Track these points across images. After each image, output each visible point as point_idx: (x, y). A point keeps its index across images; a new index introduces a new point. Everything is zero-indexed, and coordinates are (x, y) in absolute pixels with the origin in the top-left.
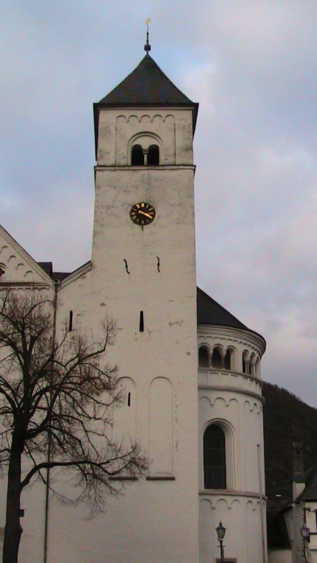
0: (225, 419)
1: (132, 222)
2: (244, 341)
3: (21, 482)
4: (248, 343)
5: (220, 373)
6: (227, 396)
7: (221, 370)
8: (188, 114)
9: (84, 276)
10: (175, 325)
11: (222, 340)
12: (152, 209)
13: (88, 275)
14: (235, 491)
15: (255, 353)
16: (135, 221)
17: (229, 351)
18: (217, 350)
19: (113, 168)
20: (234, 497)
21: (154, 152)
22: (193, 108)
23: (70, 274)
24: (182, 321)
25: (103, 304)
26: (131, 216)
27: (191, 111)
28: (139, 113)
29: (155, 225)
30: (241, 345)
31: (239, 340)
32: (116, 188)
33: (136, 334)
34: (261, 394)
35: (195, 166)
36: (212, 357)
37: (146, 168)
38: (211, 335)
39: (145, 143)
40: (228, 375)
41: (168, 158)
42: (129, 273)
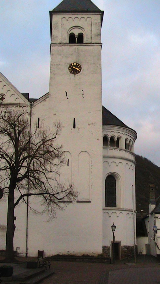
2: (126, 134)
3: (15, 203)
4: (128, 134)
6: (117, 161)
16: (71, 72)
17: (118, 139)
18: (112, 138)
19: (60, 45)
20: (119, 211)
21: (81, 36)
22: (101, 14)
24: (95, 123)
25: (55, 115)
26: (69, 69)
27: (100, 15)
28: (73, 16)
29: (81, 74)
32: (61, 55)
33: (71, 130)
35: (102, 44)
36: (110, 141)
39: (76, 32)
40: (118, 150)
42: (68, 99)
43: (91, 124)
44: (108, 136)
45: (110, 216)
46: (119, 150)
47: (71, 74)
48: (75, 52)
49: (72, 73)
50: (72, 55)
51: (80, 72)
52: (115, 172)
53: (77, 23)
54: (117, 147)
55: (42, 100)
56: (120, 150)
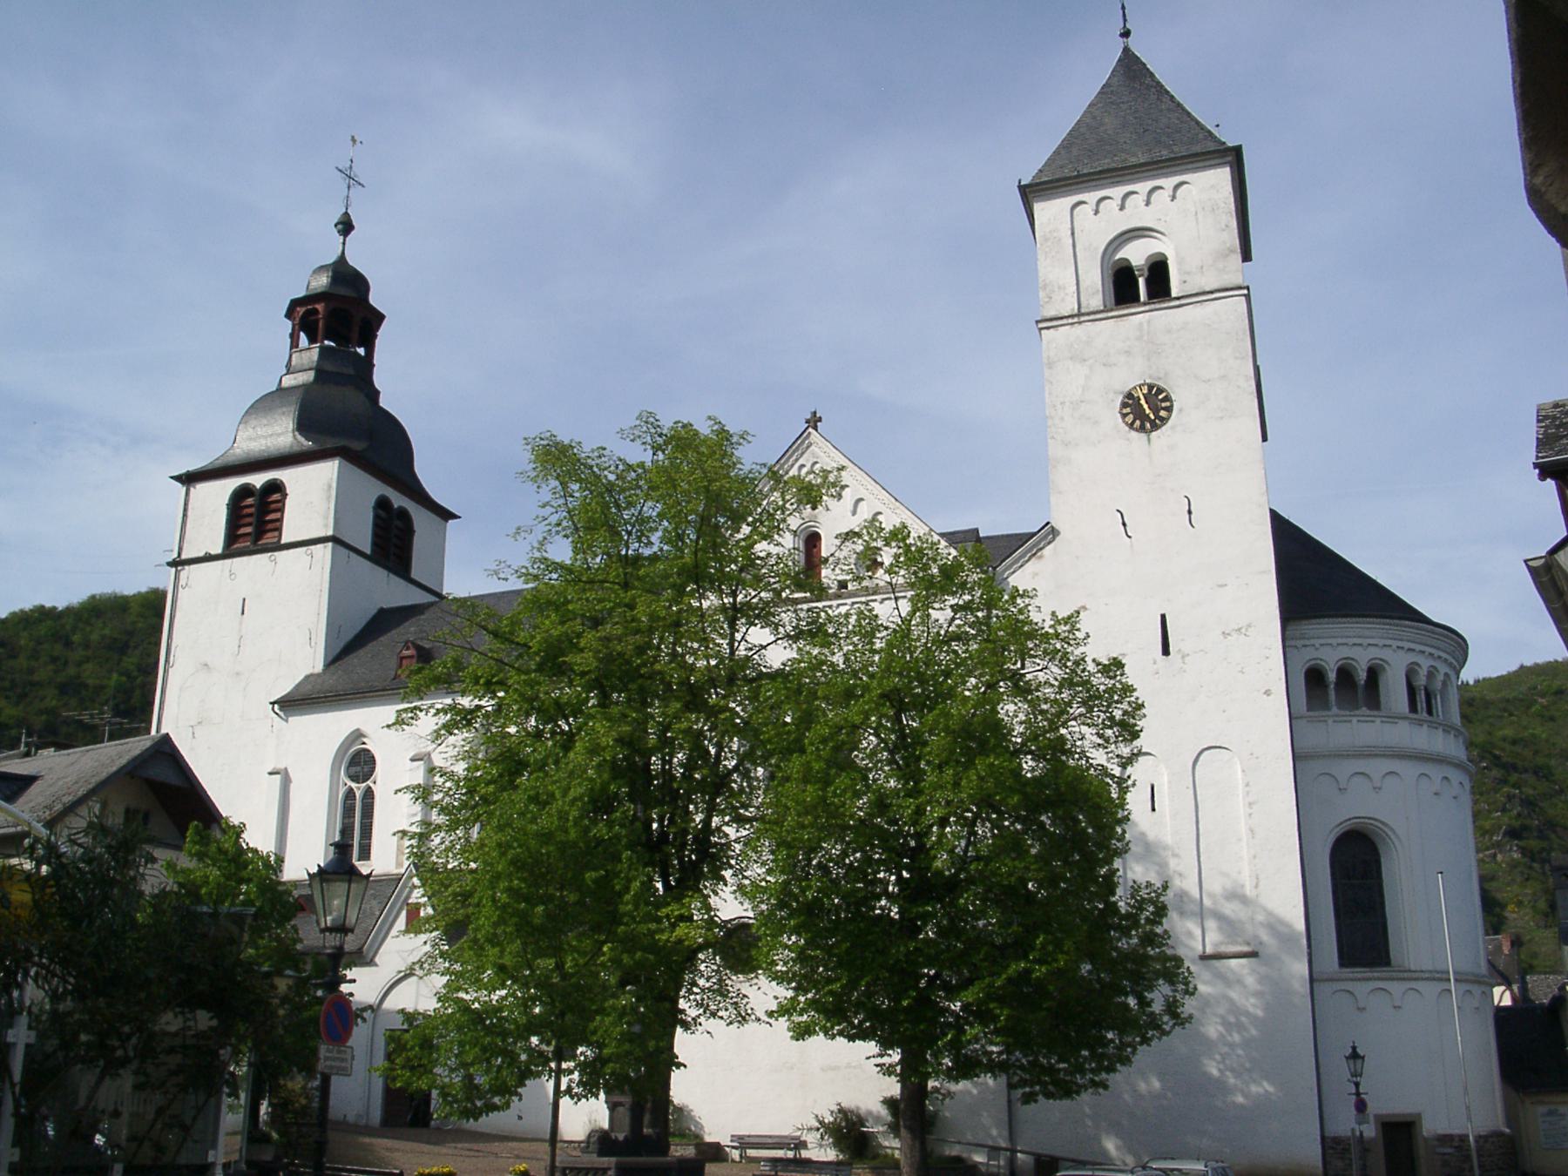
0: (1376, 817)
1: (1127, 428)
2: (1407, 645)
4: (1418, 647)
5: (1355, 720)
6: (1378, 767)
7: (1357, 712)
8: (1219, 179)
9: (1039, 554)
10: (1235, 635)
11: (1355, 648)
12: (1164, 395)
13: (1047, 551)
14: (1410, 971)
15: (1438, 664)
16: (1131, 426)
17: (1374, 673)
18: (1345, 674)
19: (1076, 320)
21: (1158, 271)
22: (1230, 159)
23: (1033, 535)
24: (1249, 626)
26: (1124, 416)
29: (1173, 428)
30: (1401, 653)
31: (1395, 644)
32: (1085, 360)
33: (1155, 663)
34: (1465, 758)
35: (1248, 288)
36: (1337, 684)
37: (1147, 308)
38: (1329, 641)
39: (1137, 254)
40: (1373, 722)
41: (1186, 278)
42: (1129, 537)
43: (1233, 633)
44: (1323, 663)
45: (1361, 1005)
46: (1382, 722)
47: (1134, 434)
48: (1139, 338)
49: (1137, 430)
50: (1128, 353)
51: (1170, 422)
52: (1369, 818)
53: (1138, 214)
54: (1370, 708)
55: (1391, 636)
56: (1384, 719)
